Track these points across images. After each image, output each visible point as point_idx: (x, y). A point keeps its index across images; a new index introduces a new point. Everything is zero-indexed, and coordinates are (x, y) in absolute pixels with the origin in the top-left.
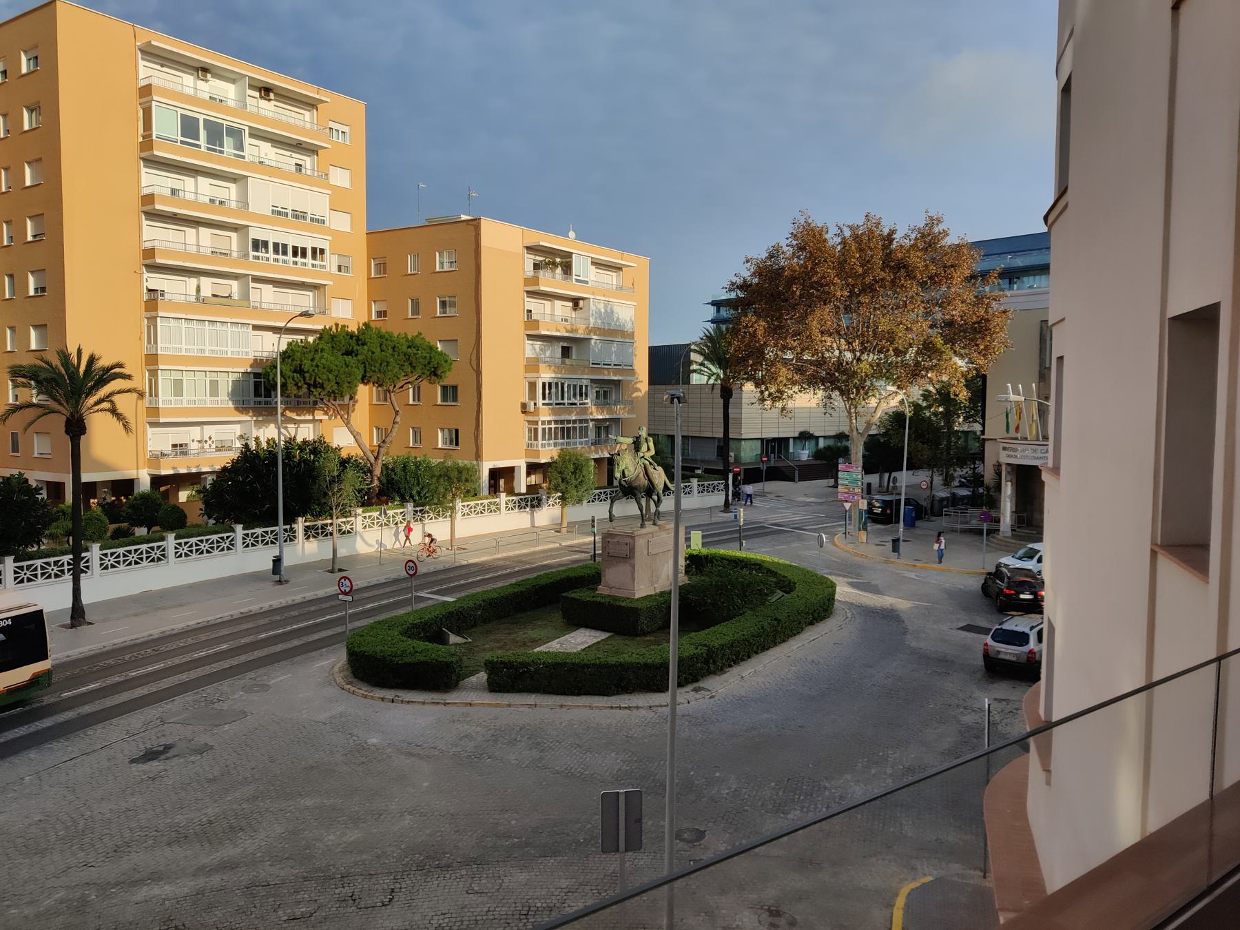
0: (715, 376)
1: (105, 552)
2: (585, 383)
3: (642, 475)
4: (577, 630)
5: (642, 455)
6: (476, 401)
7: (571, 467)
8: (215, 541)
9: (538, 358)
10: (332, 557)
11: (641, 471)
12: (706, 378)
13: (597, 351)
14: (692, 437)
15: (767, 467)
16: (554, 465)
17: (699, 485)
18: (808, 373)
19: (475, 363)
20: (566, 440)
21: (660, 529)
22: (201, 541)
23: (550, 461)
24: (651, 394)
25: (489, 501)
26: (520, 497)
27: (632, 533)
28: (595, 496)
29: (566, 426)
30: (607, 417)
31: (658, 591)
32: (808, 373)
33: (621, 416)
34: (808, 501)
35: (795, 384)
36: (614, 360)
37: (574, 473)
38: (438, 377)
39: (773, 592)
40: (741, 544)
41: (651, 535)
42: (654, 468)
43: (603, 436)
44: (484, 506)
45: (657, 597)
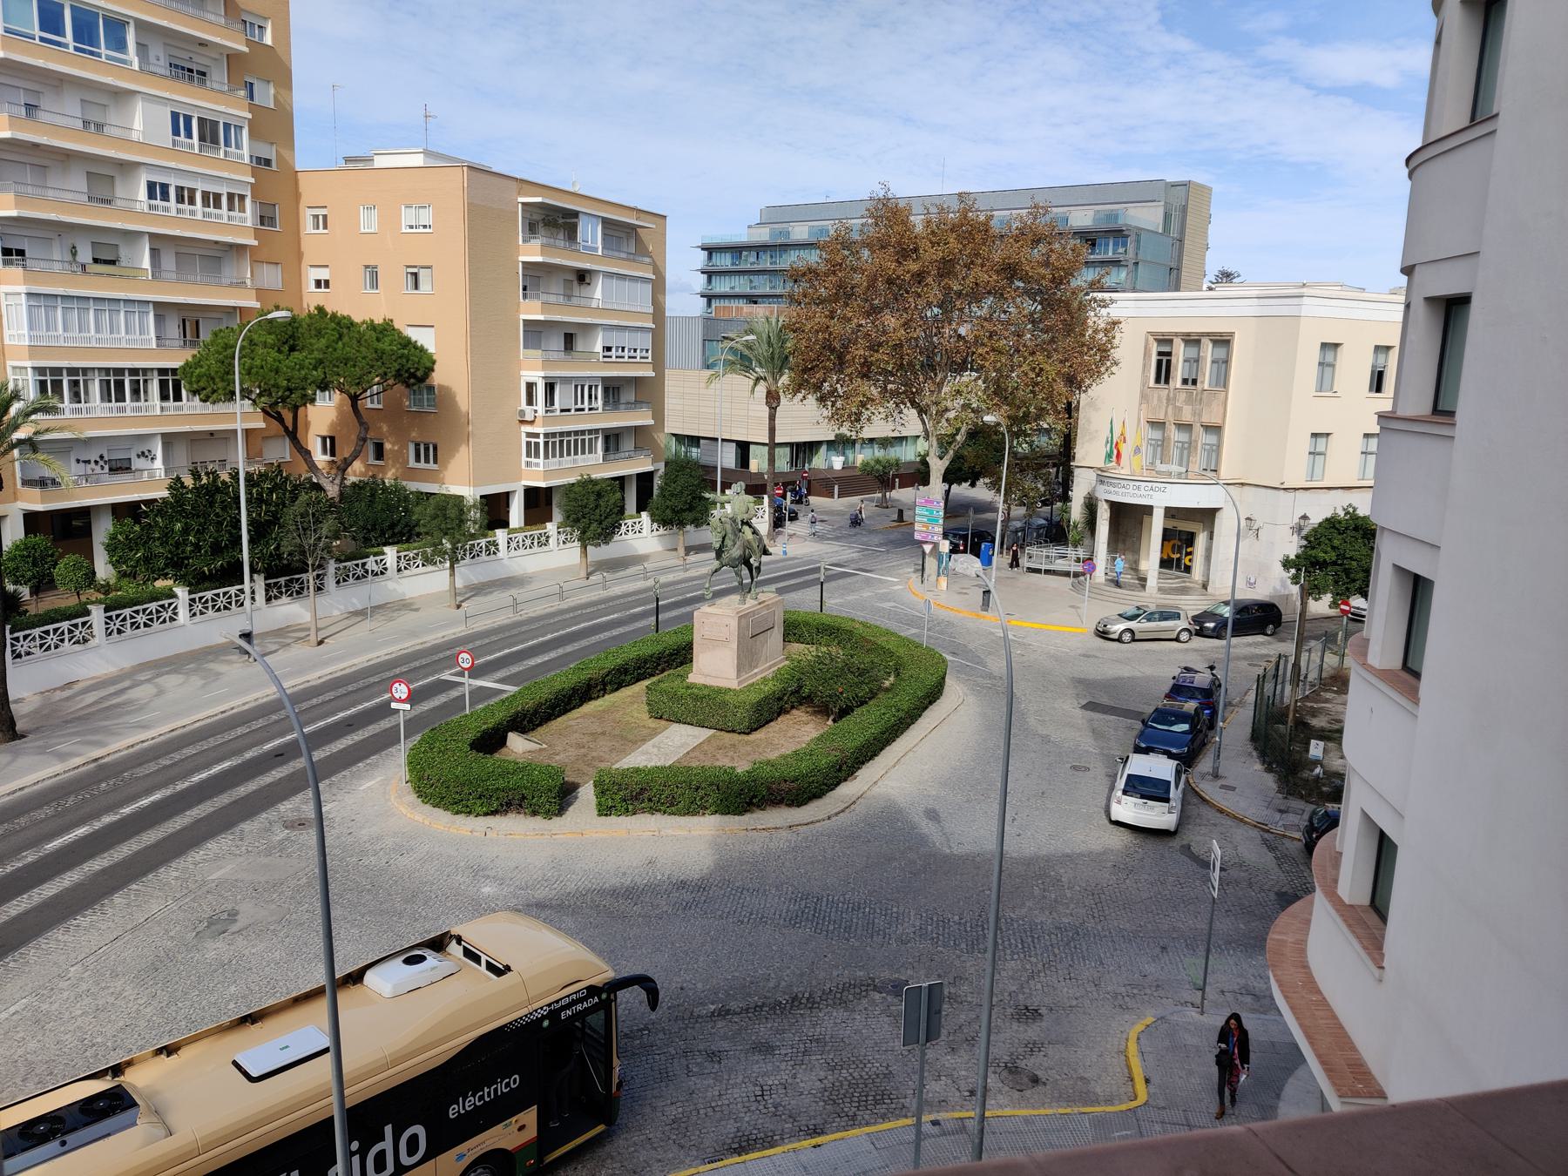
1: (108, 614)
8: (154, 611)
22: (137, 612)
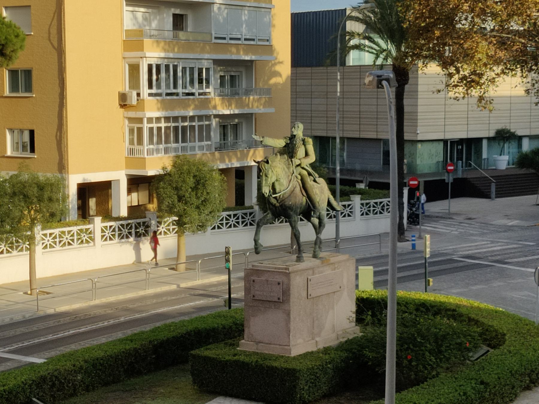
0: (384, 53)
2: (205, 64)
3: (298, 189)
4: (213, 399)
5: (298, 162)
6: (58, 90)
7: (191, 181)
9: (141, 31)
10: (29, 279)
11: (296, 184)
12: (373, 57)
13: (222, 21)
14: (348, 138)
15: (454, 179)
16: (167, 178)
17: (362, 204)
18: (515, 48)
19: (56, 39)
20: (181, 144)
21: (322, 263)
23: (162, 172)
24: (294, 78)
25: (79, 227)
26: (121, 222)
27: (286, 269)
28: (222, 220)
29: (181, 124)
30: (237, 112)
31: (321, 346)
32: (515, 48)
33: (255, 110)
34: (510, 224)
35: (498, 64)
36: (244, 32)
37: (195, 189)
38: (6, 59)
39: (476, 347)
40: (427, 283)
41: (311, 272)
42: (315, 181)
43: (230, 138)
44: (72, 236)
45: (321, 355)
